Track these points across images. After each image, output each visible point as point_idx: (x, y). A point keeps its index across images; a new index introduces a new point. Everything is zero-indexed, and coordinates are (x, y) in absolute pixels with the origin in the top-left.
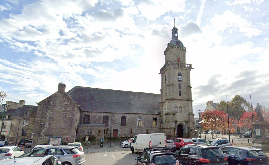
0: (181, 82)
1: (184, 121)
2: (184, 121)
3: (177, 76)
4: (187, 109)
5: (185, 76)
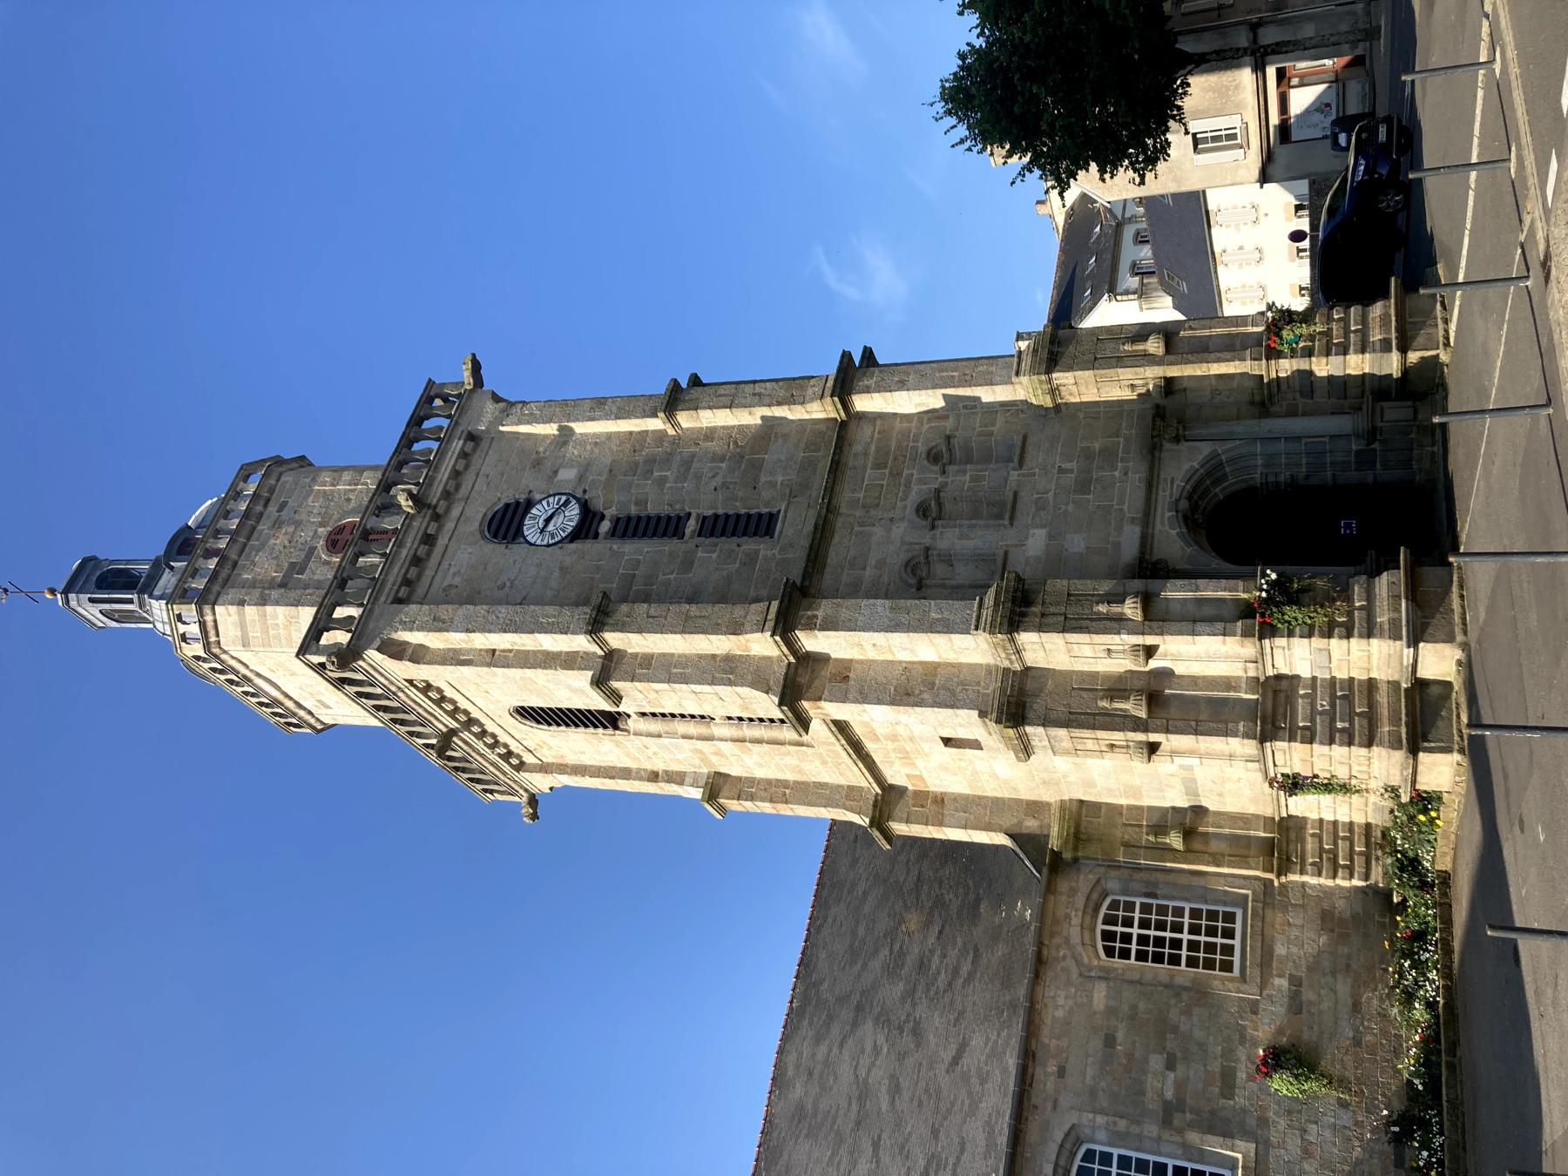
0: (598, 504)
1: (526, 790)
2: (526, 790)
3: (518, 549)
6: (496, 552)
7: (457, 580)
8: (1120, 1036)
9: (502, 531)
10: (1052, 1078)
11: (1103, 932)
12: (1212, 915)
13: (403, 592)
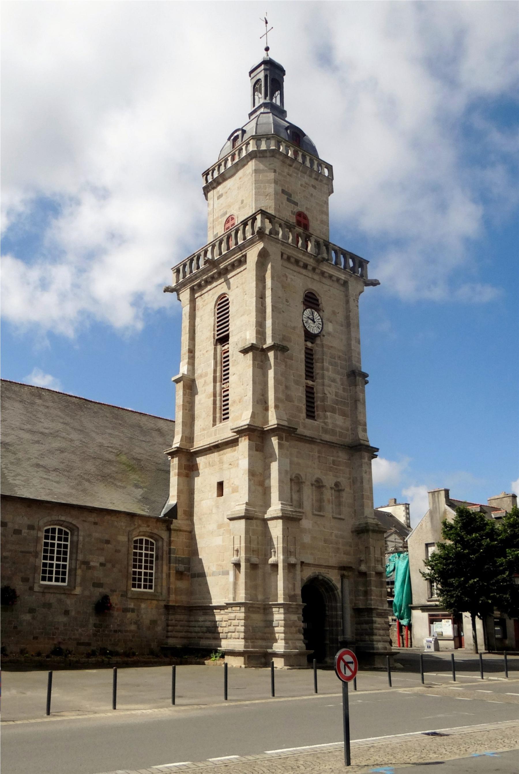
0: (318, 341)
3: (302, 306)
4: (346, 497)
5: (334, 313)
6: (300, 298)
7: (289, 280)
8: (109, 546)
9: (308, 299)
10: (93, 520)
11: (143, 539)
12: (151, 581)
13: (285, 256)
